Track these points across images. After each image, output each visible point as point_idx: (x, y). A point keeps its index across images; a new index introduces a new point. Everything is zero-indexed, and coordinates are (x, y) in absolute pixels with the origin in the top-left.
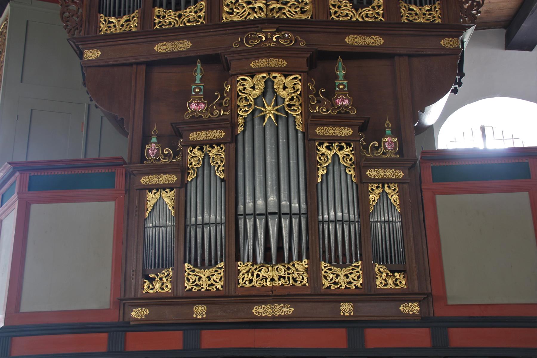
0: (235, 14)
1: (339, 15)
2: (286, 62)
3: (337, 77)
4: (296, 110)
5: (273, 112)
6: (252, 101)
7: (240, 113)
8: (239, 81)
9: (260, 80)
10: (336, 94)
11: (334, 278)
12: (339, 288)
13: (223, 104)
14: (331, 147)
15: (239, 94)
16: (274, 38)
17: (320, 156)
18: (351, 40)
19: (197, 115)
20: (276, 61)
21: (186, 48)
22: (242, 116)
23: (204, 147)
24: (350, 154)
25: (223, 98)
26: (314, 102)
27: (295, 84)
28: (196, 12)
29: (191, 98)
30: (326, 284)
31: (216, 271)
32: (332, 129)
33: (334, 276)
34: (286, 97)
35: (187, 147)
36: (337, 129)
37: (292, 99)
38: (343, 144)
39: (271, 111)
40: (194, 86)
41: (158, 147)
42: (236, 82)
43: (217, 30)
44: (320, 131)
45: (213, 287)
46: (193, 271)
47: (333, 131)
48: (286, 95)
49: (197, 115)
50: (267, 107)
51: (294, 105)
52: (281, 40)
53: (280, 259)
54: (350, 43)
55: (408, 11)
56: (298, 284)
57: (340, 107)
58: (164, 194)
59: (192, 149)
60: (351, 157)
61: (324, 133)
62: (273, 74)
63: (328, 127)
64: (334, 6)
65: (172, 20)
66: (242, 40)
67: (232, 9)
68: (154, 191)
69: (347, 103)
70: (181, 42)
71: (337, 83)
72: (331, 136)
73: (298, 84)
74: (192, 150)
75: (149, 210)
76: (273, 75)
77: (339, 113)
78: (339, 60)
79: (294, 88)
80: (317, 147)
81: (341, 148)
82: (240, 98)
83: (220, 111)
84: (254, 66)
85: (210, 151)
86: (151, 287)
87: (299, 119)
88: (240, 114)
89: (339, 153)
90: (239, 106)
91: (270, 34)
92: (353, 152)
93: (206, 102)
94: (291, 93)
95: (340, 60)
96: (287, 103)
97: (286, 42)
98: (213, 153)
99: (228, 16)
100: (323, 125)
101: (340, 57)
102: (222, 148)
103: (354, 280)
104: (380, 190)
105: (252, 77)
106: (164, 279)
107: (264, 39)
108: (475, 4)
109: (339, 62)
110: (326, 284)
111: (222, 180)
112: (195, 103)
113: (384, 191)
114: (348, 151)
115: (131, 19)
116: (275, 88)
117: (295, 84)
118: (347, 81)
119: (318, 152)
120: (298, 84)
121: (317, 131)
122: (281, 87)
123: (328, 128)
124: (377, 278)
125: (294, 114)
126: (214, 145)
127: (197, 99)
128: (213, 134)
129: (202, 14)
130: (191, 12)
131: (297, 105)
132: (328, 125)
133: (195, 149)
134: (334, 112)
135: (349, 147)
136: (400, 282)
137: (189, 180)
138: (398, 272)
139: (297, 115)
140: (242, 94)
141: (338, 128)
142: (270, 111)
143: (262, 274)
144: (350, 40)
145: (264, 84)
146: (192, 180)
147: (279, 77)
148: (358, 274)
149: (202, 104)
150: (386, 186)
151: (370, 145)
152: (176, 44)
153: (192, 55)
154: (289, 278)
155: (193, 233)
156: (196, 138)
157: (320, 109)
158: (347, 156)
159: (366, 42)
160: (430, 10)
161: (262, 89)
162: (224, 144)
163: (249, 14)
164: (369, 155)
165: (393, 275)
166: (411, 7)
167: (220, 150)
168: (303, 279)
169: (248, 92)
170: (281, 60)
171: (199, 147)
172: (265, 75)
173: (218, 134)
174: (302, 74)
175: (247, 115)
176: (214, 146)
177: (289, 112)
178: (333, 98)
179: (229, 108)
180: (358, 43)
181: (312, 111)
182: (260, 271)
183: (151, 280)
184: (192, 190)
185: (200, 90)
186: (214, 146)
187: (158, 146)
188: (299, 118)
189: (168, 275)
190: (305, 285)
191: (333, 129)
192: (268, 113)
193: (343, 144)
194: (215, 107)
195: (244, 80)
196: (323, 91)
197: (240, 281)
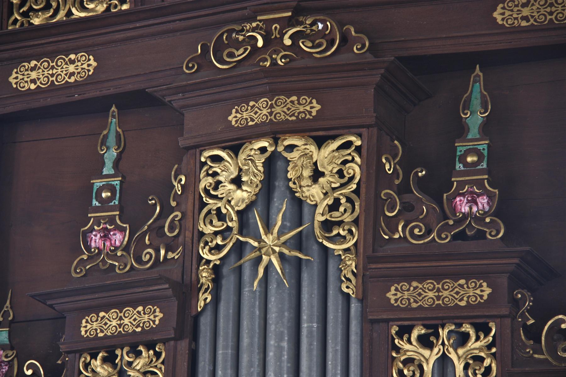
2: (317, 103)
4: (344, 237)
5: (277, 249)
6: (234, 219)
7: (205, 254)
8: (205, 163)
10: (455, 183)
13: (166, 230)
14: (432, 339)
15: (204, 199)
16: (287, 37)
17: (401, 365)
18: (511, 13)
19: (103, 265)
20: (292, 102)
21: (84, 73)
22: (208, 262)
23: (118, 352)
24: (485, 356)
25: (166, 210)
26: (392, 210)
27: (345, 162)
29: (91, 217)
32: (432, 286)
34: (319, 201)
35: (77, 355)
36: (447, 287)
37: (335, 206)
38: (467, 328)
39: (274, 245)
40: (99, 184)
41: (10, 359)
42: (198, 165)
43: (151, 22)
44: (399, 295)
47: (436, 294)
48: (319, 198)
49: (103, 265)
50: (264, 237)
51: (340, 223)
52: (303, 43)
54: (507, 22)
57: (465, 216)
59: (89, 359)
60: (487, 362)
61: (409, 300)
62: (285, 139)
63: (421, 283)
66: (205, 49)
69: (485, 205)
70: (73, 59)
71: (461, 148)
72: (430, 308)
73: (353, 160)
74: (89, 363)
76: (286, 143)
77: (461, 236)
78: (474, 77)
79: (340, 173)
80: (393, 339)
82: (205, 210)
83: (158, 251)
84: (236, 121)
85: (130, 364)
87: (350, 262)
88: (205, 256)
90: (202, 234)
91: (278, 27)
92: (494, 350)
93: (125, 225)
94: (334, 189)
95: (478, 76)
96: (322, 219)
97: (320, 45)
98: (138, 368)
100: (409, 278)
101: (478, 66)
105: (235, 150)
107: (260, 43)
109: (475, 82)
112: (99, 231)
114: (480, 349)
116: (291, 180)
117: (345, 162)
118: (487, 142)
119: (394, 355)
120: (353, 160)
121: (391, 295)
122: (307, 173)
123: (420, 286)
125: (337, 248)
126: (141, 348)
127: (103, 220)
128: (135, 316)
131: (348, 223)
132: (421, 278)
133: (96, 359)
134: (443, 236)
135: (482, 337)
139: (347, 250)
140: (211, 201)
141: (449, 283)
144: (507, 13)
145: (262, 169)
147: (304, 147)
149: (116, 232)
151: (545, 325)
152: (59, 64)
153: (97, 93)
156: (468, 287)
157: (408, 229)
158: (477, 363)
159: (555, 14)
161: (258, 182)
162: (164, 344)
164: (542, 357)
167: (154, 360)
169: (224, 195)
170: (304, 99)
171: (106, 352)
172: (265, 144)
173: (147, 316)
174: (364, 131)
175: (220, 259)
176: (139, 348)
177: (326, 243)
178: (445, 195)
179: (181, 239)
180: (532, 20)
181: (387, 237)
185: (111, 194)
186: (139, 348)
187: (9, 355)
188: (349, 260)
191: (437, 286)
192: (267, 254)
193: (467, 328)
194: (149, 240)
195: (217, 159)
196: (420, 174)
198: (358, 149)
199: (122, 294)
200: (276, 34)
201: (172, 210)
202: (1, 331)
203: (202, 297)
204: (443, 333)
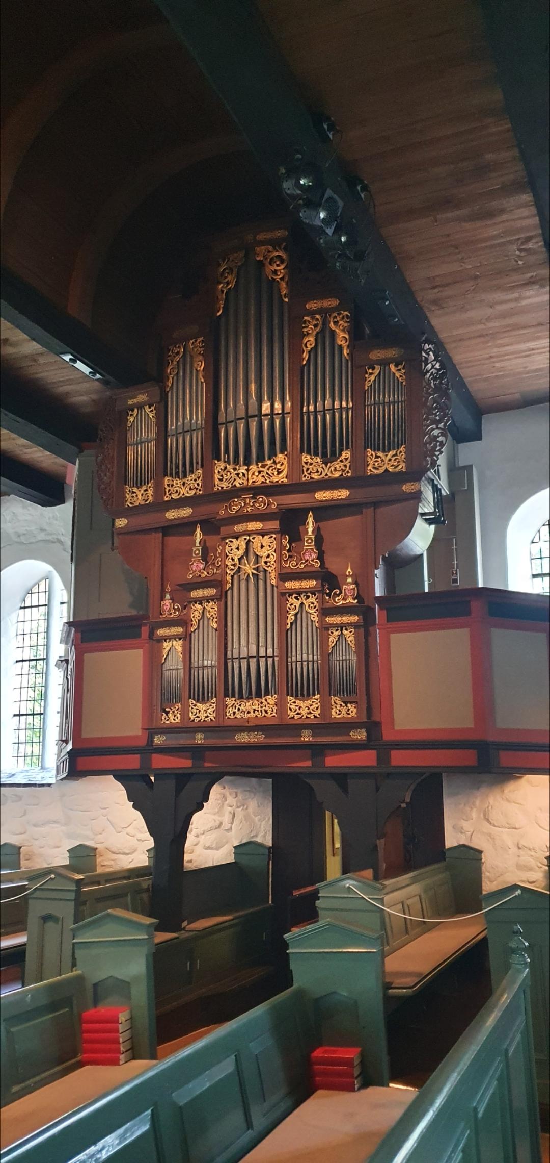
0: (224, 480)
1: (311, 472)
3: (307, 532)
7: (228, 571)
9: (242, 543)
11: (298, 709)
12: (301, 718)
25: (216, 557)
28: (195, 480)
30: (291, 714)
31: (210, 705)
33: (297, 708)
45: (209, 718)
46: (195, 706)
53: (259, 695)
55: (375, 458)
56: (269, 715)
58: (175, 642)
64: (306, 463)
65: (178, 489)
67: (222, 476)
68: (168, 641)
75: (165, 656)
79: (270, 546)
81: (308, 597)
83: (214, 570)
86: (167, 718)
89: (304, 602)
90: (227, 565)
99: (219, 482)
102: (215, 603)
103: (314, 711)
104: (338, 633)
106: (176, 712)
108: (438, 444)
110: (291, 714)
111: (216, 630)
113: (342, 633)
115: (398, 454)
122: (260, 545)
124: (332, 709)
129: (199, 481)
130: (191, 480)
136: (352, 712)
137: (192, 630)
138: (351, 703)
142: (249, 569)
143: (242, 708)
146: (195, 630)
148: (317, 706)
150: (344, 628)
154: (261, 711)
155: (196, 674)
160: (396, 455)
163: (235, 480)
165: (347, 706)
166: (378, 454)
168: (273, 711)
182: (240, 705)
183: (167, 713)
184: (194, 637)
189: (178, 709)
190: (274, 716)
197: (228, 714)
198: (275, 538)
199: (242, 625)
200: (248, 502)
201: (218, 557)
202: (479, 1160)
203: (228, 585)
204: (302, 596)
